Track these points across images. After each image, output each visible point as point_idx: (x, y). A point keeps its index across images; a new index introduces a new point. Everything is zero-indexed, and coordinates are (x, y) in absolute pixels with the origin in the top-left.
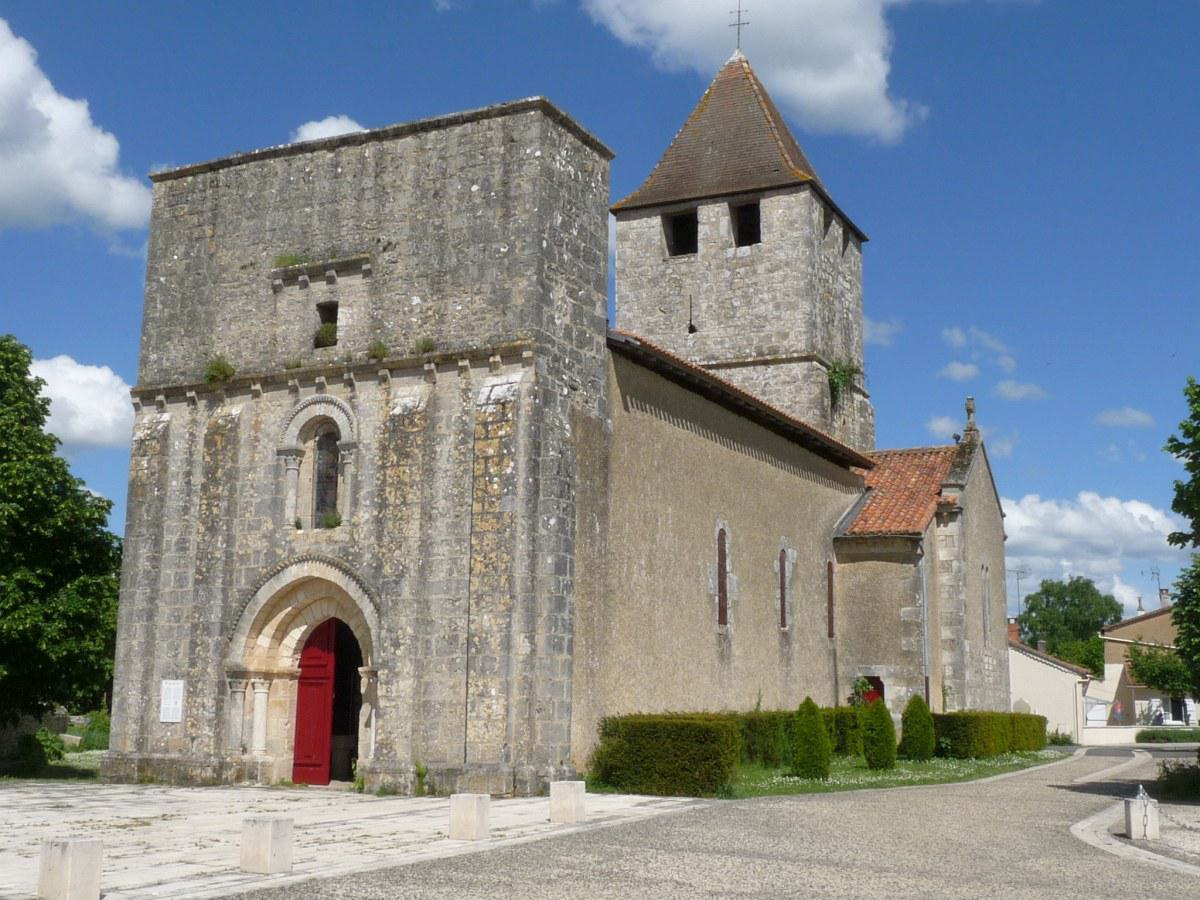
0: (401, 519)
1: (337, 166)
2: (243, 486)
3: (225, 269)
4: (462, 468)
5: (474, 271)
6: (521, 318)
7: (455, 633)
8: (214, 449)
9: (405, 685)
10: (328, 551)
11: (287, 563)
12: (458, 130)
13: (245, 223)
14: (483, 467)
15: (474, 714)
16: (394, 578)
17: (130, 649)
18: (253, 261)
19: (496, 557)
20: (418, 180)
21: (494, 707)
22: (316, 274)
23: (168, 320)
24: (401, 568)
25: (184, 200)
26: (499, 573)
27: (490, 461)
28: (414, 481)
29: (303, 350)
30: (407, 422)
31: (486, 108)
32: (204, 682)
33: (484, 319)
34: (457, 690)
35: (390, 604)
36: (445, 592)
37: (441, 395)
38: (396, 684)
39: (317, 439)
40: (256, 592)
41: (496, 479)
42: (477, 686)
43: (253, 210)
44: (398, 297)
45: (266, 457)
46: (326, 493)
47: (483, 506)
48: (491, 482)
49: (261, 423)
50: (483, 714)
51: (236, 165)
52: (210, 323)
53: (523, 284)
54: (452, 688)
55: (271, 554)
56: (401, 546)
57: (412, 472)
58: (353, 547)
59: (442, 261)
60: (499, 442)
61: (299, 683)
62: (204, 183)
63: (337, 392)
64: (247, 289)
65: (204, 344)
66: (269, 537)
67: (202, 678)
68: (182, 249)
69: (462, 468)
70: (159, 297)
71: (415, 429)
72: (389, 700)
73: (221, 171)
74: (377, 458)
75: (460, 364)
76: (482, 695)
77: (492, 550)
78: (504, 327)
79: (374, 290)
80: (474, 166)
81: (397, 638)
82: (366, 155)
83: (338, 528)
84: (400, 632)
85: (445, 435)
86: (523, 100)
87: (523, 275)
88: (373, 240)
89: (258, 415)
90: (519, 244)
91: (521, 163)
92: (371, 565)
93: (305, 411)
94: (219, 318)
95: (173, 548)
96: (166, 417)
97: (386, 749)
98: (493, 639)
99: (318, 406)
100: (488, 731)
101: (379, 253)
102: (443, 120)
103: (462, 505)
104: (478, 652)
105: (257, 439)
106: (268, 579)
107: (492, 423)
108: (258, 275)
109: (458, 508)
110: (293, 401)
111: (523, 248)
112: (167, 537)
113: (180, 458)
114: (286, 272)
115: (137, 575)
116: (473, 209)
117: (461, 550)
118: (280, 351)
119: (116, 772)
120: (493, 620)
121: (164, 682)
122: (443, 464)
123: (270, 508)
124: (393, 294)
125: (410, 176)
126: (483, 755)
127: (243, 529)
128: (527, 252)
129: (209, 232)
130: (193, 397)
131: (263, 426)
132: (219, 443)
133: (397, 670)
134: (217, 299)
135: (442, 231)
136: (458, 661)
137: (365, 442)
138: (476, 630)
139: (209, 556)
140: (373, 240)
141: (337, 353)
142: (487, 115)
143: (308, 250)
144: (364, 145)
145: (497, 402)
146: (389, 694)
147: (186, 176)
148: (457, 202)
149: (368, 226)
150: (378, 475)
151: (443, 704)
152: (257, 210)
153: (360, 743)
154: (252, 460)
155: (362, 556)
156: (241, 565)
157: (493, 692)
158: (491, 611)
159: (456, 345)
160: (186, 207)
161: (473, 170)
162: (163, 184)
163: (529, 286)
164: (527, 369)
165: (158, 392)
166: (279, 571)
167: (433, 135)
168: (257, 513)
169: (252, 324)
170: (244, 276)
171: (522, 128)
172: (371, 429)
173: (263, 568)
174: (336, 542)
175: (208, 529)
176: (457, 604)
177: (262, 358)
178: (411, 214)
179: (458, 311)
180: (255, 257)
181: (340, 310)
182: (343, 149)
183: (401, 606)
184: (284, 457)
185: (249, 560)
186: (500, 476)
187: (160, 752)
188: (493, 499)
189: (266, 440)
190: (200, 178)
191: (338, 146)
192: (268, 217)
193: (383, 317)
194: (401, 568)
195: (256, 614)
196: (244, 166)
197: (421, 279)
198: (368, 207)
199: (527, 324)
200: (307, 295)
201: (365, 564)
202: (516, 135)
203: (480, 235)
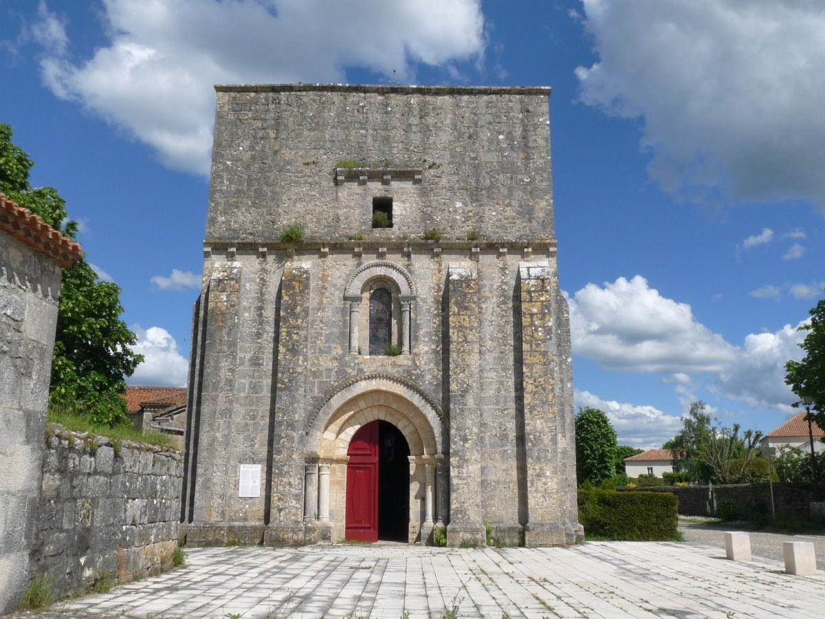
0: (464, 351)
1: (387, 105)
2: (314, 321)
3: (289, 163)
4: (504, 320)
5: (504, 191)
6: (543, 226)
7: (505, 432)
8: (291, 292)
9: (473, 469)
10: (391, 371)
11: (359, 379)
12: (485, 98)
13: (306, 132)
14: (529, 320)
15: (533, 489)
16: (460, 393)
17: (214, 440)
18: (316, 161)
19: (544, 381)
20: (455, 125)
21: (550, 484)
22: (373, 176)
23: (235, 193)
24: (465, 386)
25: (248, 108)
26: (547, 392)
27: (535, 316)
28: (473, 326)
29: (363, 228)
30: (464, 285)
31: (509, 88)
32: (290, 466)
33: (515, 223)
34: (510, 472)
35: (458, 411)
36: (494, 404)
37: (483, 270)
38: (466, 468)
39: (372, 291)
40: (329, 399)
41: (540, 329)
42: (534, 469)
43: (313, 125)
44: (443, 200)
45: (333, 301)
46: (377, 331)
47: (531, 346)
48: (536, 330)
49: (328, 276)
50: (540, 488)
51: (296, 91)
52: (275, 198)
53: (543, 204)
54: (505, 470)
55: (341, 373)
56: (464, 370)
57: (470, 320)
58: (415, 370)
59: (478, 181)
60: (541, 305)
61: (348, 467)
62: (266, 99)
63: (395, 259)
64: (310, 180)
65: (271, 214)
66: (340, 359)
67: (287, 463)
68: (247, 143)
69: (504, 320)
70: (225, 176)
71: (472, 291)
72: (460, 479)
73: (282, 93)
74: (433, 309)
75: (501, 250)
76: (539, 475)
77: (540, 376)
78: (530, 230)
79: (424, 193)
80: (500, 123)
81: (465, 434)
82: (412, 102)
83: (401, 356)
84: (467, 431)
85: (488, 298)
86: (538, 87)
87: (543, 198)
88: (420, 159)
89: (324, 270)
90: (538, 178)
91: (536, 127)
92: (432, 383)
93: (368, 271)
94: (284, 197)
95: (247, 363)
96: (237, 264)
97: (461, 514)
98: (545, 436)
99: (379, 269)
100: (546, 500)
101: (426, 169)
102: (476, 89)
103: (505, 345)
104: (534, 445)
105: (324, 288)
106: (341, 390)
107: (534, 291)
108: (320, 171)
109: (503, 347)
110: (356, 262)
111: (542, 181)
112: (240, 355)
113: (252, 296)
114: (350, 172)
115: (219, 382)
116: (501, 150)
117: (507, 375)
118: (343, 226)
119: (204, 538)
120: (544, 424)
121: (242, 466)
122: (488, 316)
123: (338, 339)
124: (440, 198)
125: (448, 121)
126: (542, 517)
127: (315, 353)
128: (544, 184)
129: (272, 134)
130: (265, 252)
131: (329, 278)
132: (297, 287)
133: (466, 458)
134: (283, 183)
135: (477, 161)
136: (509, 451)
137: (422, 297)
138: (531, 430)
139: (291, 371)
140: (420, 159)
141: (394, 233)
142: (509, 92)
143: (364, 159)
144: (410, 96)
145: (537, 278)
146: (461, 475)
147: (249, 92)
148: (488, 144)
149: (416, 150)
150: (434, 320)
151: (498, 482)
152: (318, 126)
153: (410, 510)
154: (321, 303)
155: (423, 376)
156: (314, 378)
157: (548, 473)
158: (543, 418)
159: (494, 239)
160: (250, 114)
161: (499, 125)
162: (226, 94)
163: (547, 206)
164: (550, 259)
165: (232, 245)
166: (350, 385)
167: (465, 98)
168: (327, 341)
169: (316, 205)
170: (307, 170)
171: (535, 105)
172: (426, 288)
173: (335, 381)
174: (400, 366)
175: (288, 350)
176: (506, 412)
177: (326, 230)
178: (451, 147)
179: (493, 216)
180: (317, 158)
181: (395, 204)
182: (392, 95)
183: (467, 413)
184: (349, 302)
185: (321, 375)
186: (544, 327)
187: (239, 520)
188: (539, 342)
189: (333, 289)
190: (263, 95)
191: (388, 93)
192: (327, 132)
193: (431, 212)
194: (465, 386)
195: (330, 415)
196: (304, 93)
197: (461, 191)
198: (416, 138)
199: (548, 230)
200: (365, 190)
201: (427, 382)
202: (531, 108)
203: (507, 168)
